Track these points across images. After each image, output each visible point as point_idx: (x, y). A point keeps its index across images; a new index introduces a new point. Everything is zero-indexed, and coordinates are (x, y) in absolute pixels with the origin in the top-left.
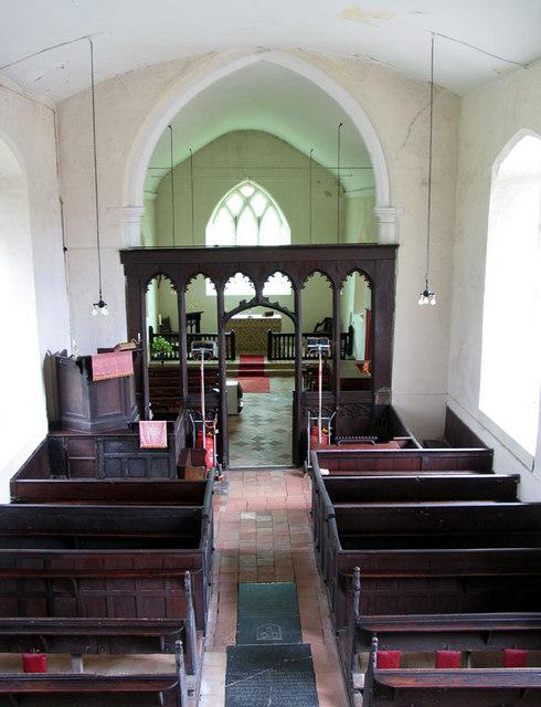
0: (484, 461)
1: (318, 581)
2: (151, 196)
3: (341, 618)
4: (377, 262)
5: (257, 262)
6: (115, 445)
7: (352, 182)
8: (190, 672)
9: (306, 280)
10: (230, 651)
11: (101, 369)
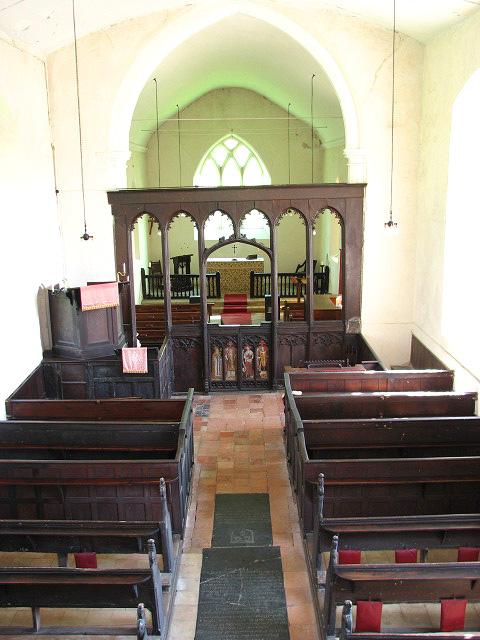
0: (446, 381)
1: (289, 491)
2: (141, 149)
3: (308, 523)
4: (347, 201)
5: (234, 201)
6: (103, 370)
7: (325, 134)
8: (166, 569)
9: (280, 217)
10: (206, 553)
11: (89, 301)
